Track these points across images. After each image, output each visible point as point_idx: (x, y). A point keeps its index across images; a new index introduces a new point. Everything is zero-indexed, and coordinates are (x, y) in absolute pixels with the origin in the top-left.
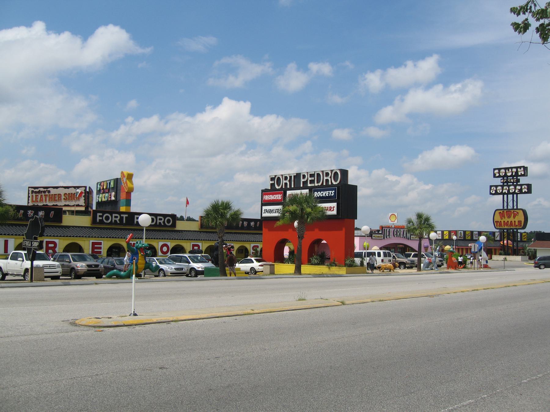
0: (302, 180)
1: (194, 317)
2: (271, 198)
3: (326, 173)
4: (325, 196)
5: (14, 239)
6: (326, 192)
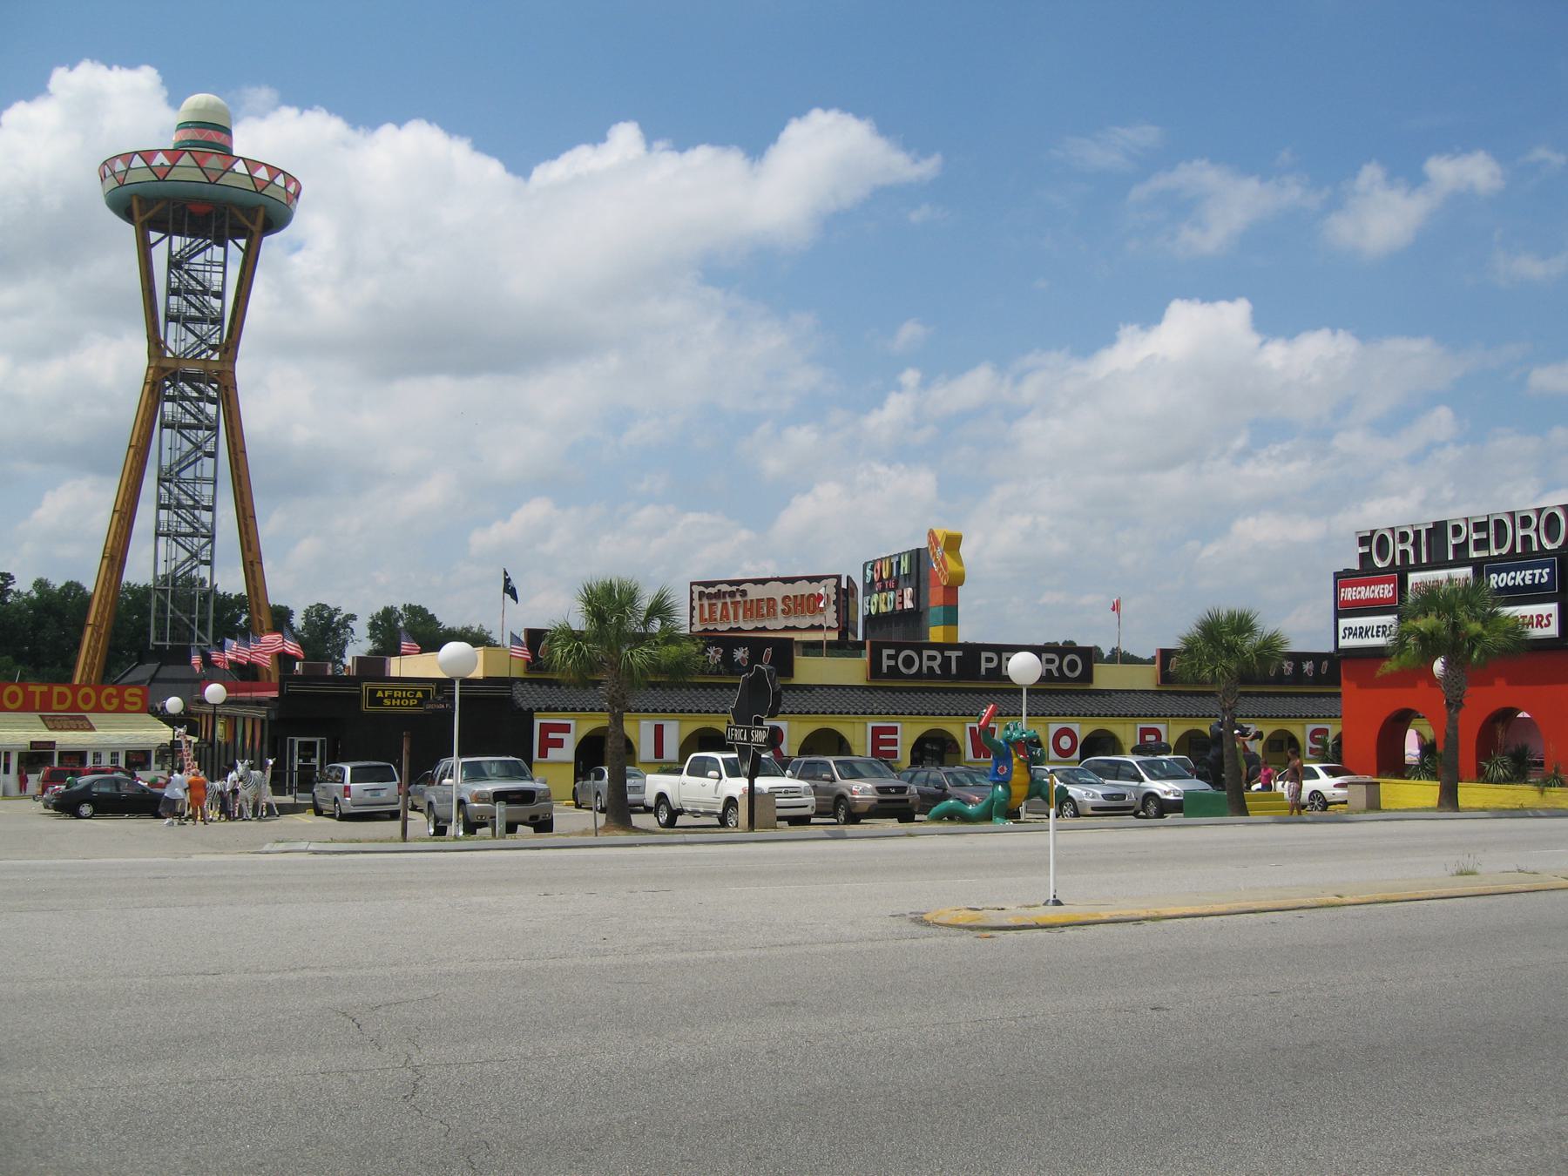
0: (1452, 541)
1: (1197, 910)
2: (1362, 593)
3: (1522, 518)
4: (1522, 584)
5: (676, 723)
6: (1523, 572)
